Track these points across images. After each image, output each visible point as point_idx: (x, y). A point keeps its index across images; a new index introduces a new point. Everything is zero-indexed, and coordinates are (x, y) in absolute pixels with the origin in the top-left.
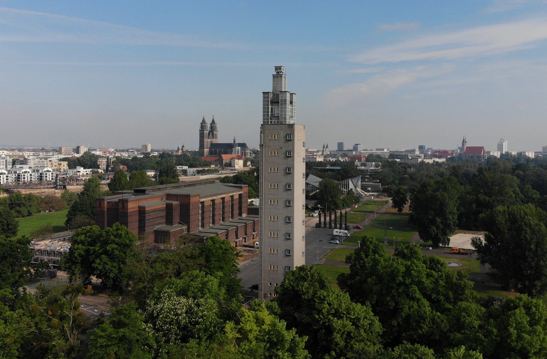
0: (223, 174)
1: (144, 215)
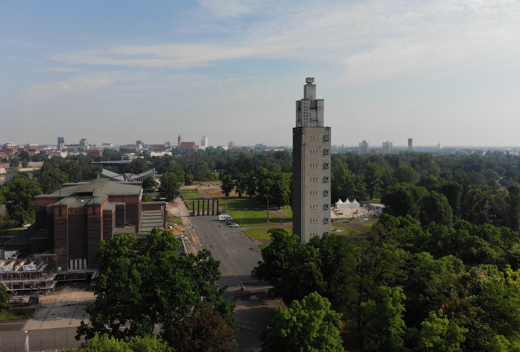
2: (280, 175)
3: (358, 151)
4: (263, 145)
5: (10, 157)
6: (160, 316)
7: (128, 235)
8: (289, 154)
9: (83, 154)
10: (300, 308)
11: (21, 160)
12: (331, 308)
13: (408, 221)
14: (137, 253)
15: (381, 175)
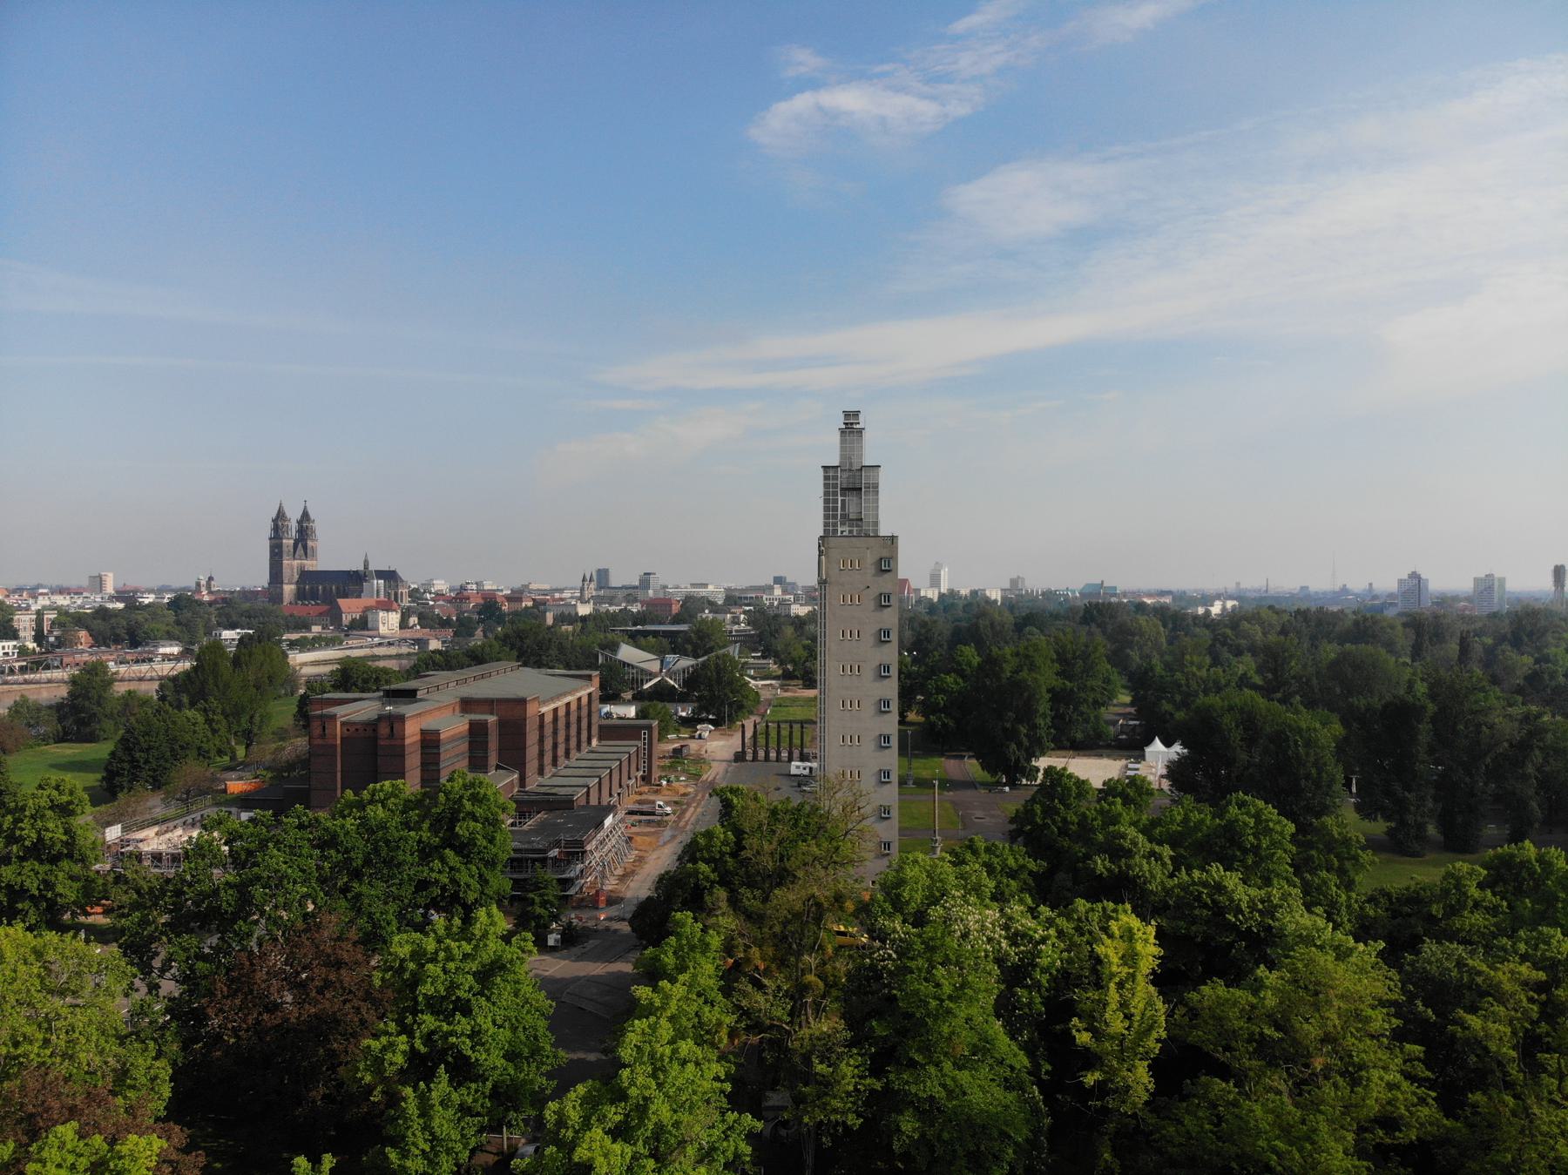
0: (351, 648)
1: (435, 751)
4: (1105, 585)
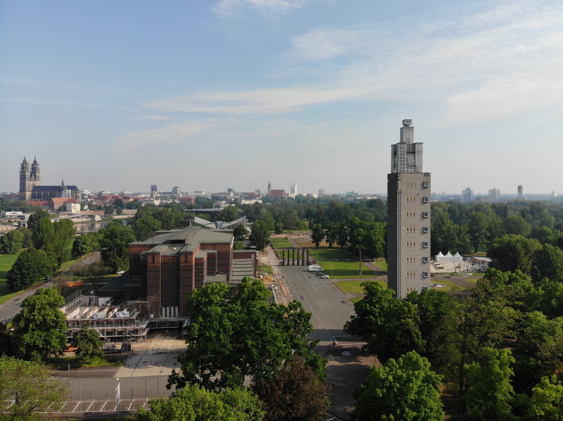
2: (373, 225)
3: (462, 200)
4: (354, 192)
5: (105, 205)
6: (251, 368)
7: (219, 283)
8: (382, 202)
9: (175, 201)
10: (396, 367)
11: (115, 208)
12: (431, 369)
13: (517, 277)
14: (228, 302)
15: (487, 226)
